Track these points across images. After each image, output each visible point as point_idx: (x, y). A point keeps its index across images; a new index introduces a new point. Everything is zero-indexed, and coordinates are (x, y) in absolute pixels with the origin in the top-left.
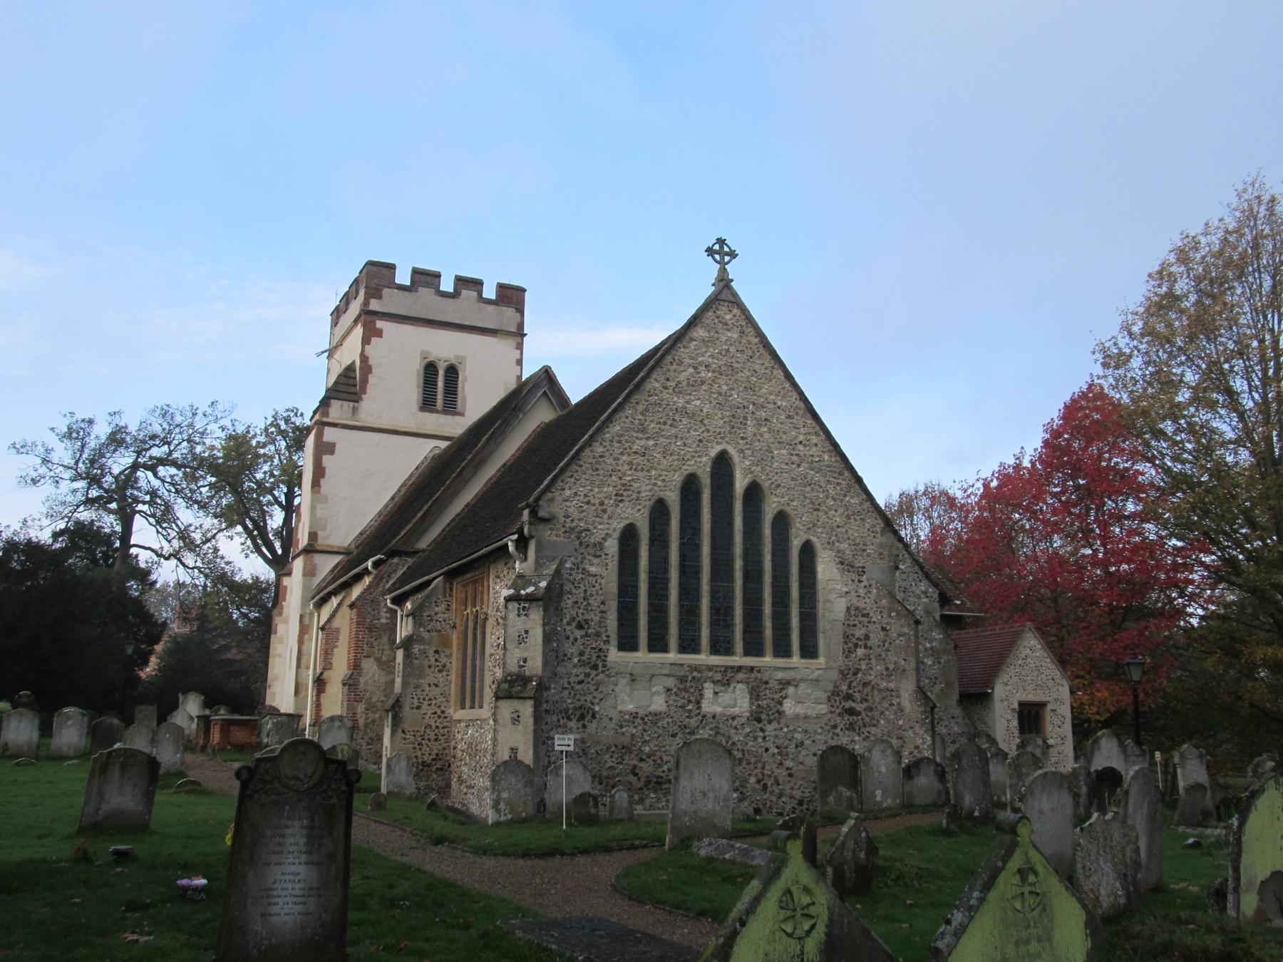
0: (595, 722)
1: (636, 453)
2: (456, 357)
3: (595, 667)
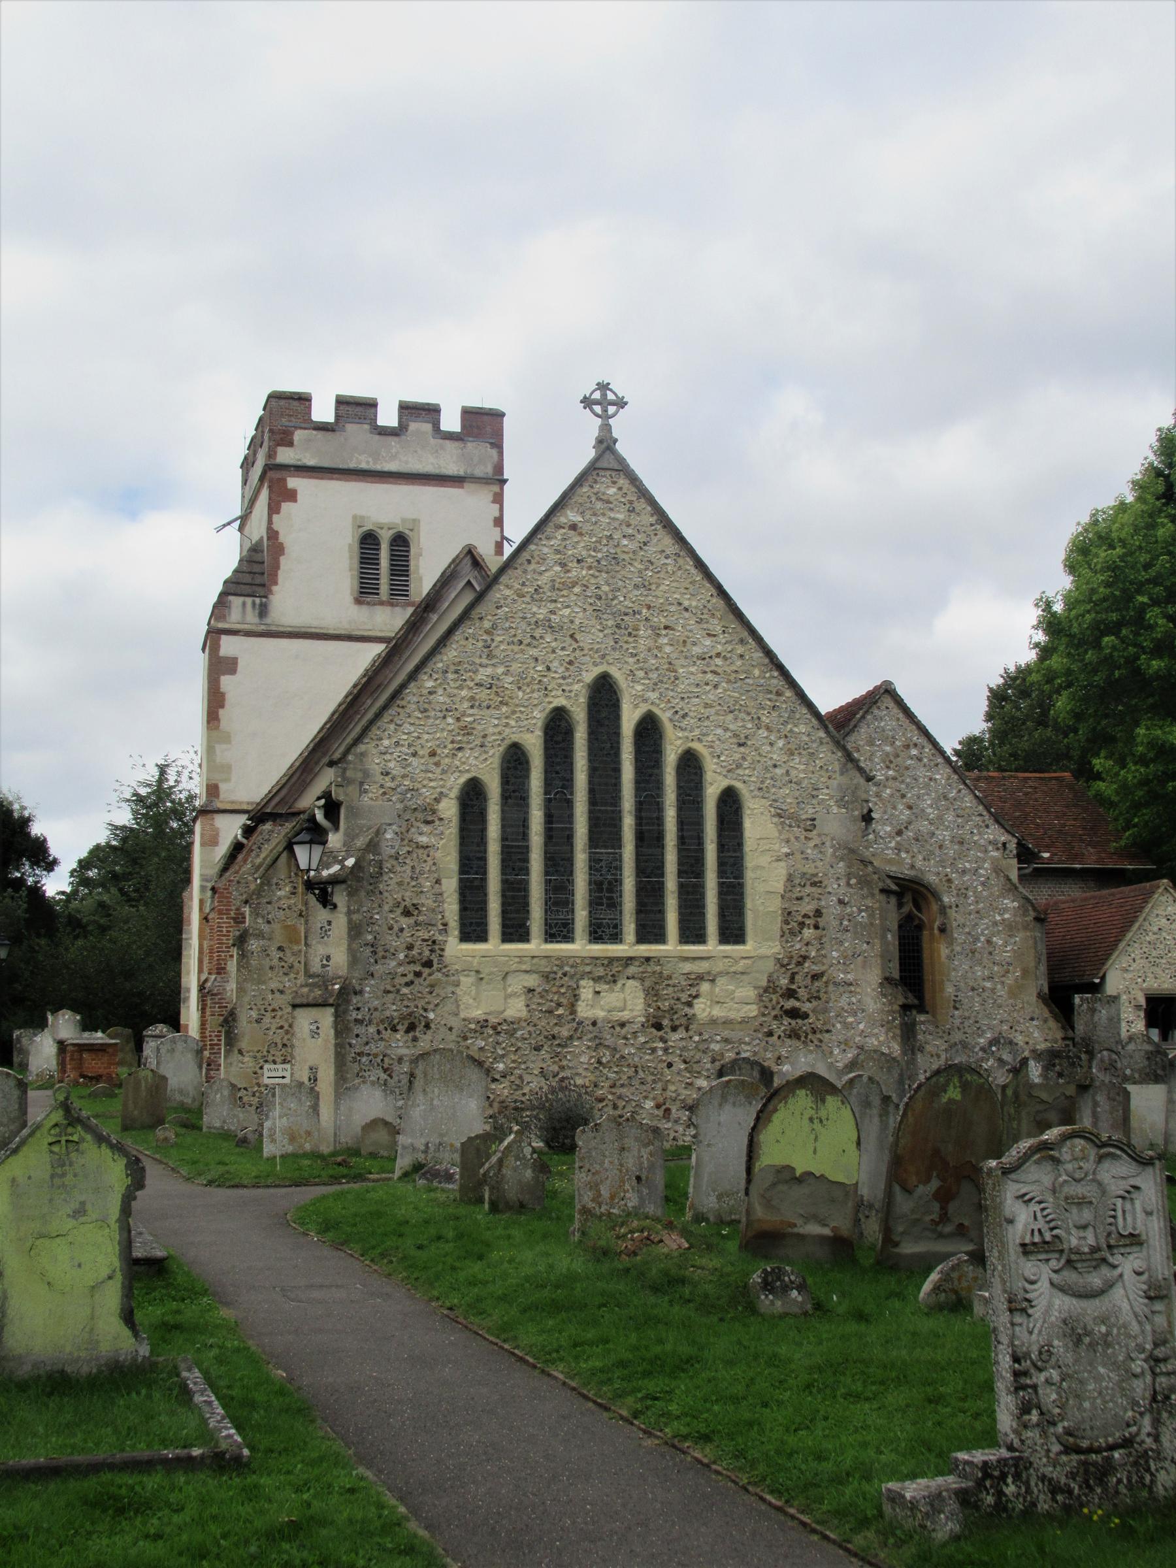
0: (429, 1032)
1: (479, 685)
2: (404, 521)
3: (428, 964)
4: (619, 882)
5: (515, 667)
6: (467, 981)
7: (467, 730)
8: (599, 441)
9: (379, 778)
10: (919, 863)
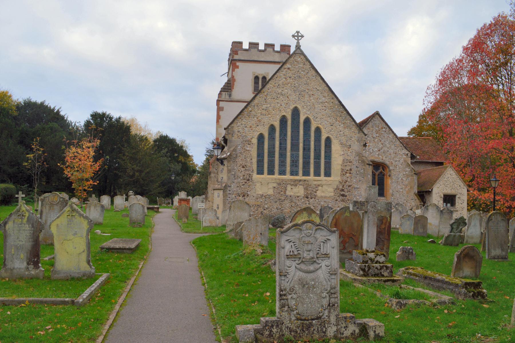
3: (248, 180)
4: (298, 160)
5: (272, 105)
6: (258, 185)
7: (260, 121)
8: (296, 46)
9: (237, 133)
10: (384, 158)
